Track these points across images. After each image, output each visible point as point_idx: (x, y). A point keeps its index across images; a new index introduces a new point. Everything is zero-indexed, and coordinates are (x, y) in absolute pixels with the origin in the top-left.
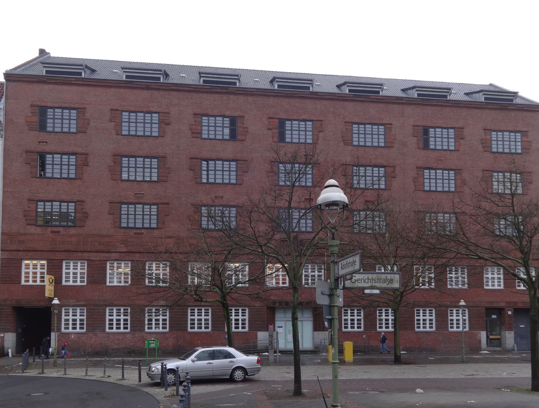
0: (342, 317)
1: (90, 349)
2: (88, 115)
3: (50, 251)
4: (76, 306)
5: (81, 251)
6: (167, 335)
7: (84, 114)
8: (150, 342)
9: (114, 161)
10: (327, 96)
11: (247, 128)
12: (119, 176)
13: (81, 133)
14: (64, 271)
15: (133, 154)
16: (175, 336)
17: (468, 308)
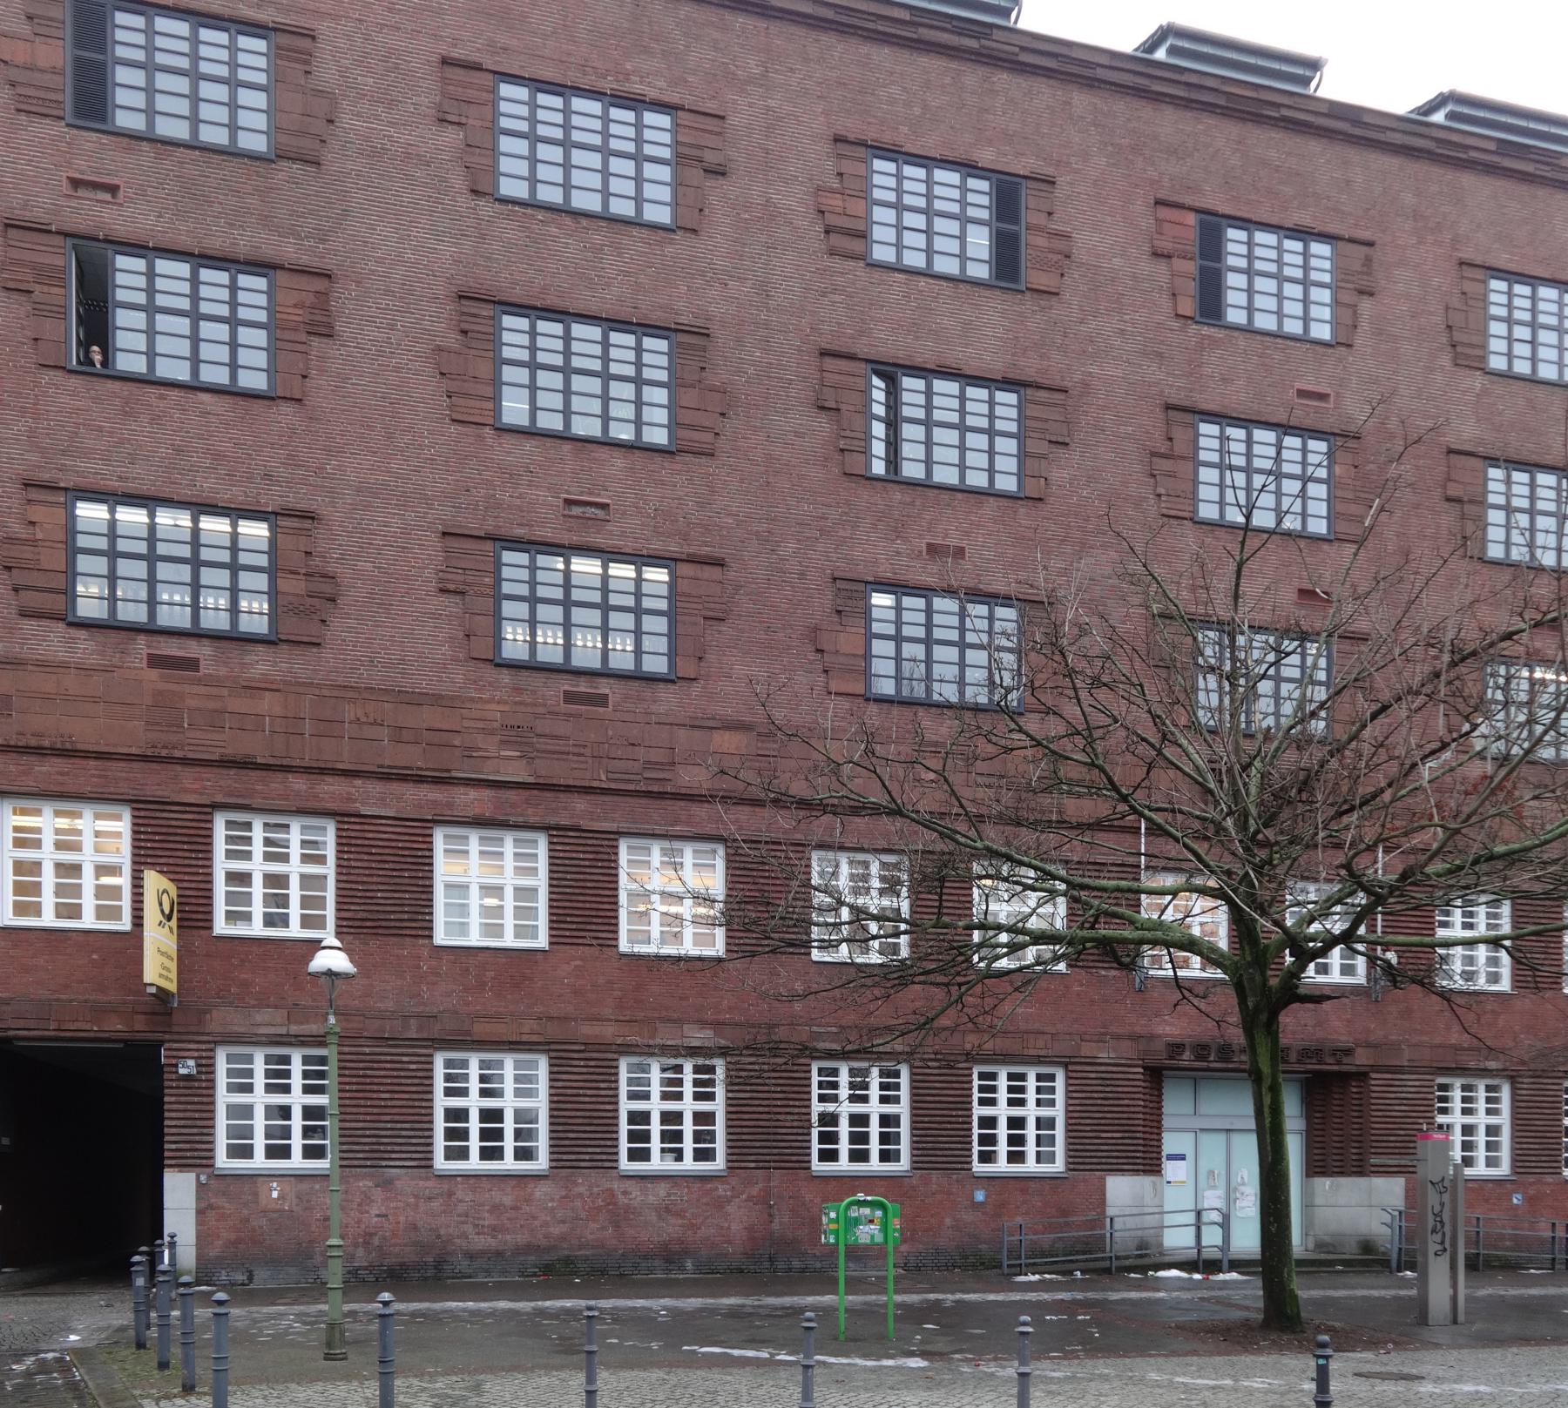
0: (809, 1107)
1: (360, 1252)
2: (326, 73)
3: (144, 758)
4: (290, 1044)
5: (307, 770)
6: (722, 1190)
7: (307, 62)
8: (854, 1213)
9: (465, 326)
10: (1398, 136)
11: (1066, 236)
12: (490, 405)
13: (294, 160)
14: (221, 866)
15: (552, 300)
16: (755, 1191)
17: (1066, 1065)
